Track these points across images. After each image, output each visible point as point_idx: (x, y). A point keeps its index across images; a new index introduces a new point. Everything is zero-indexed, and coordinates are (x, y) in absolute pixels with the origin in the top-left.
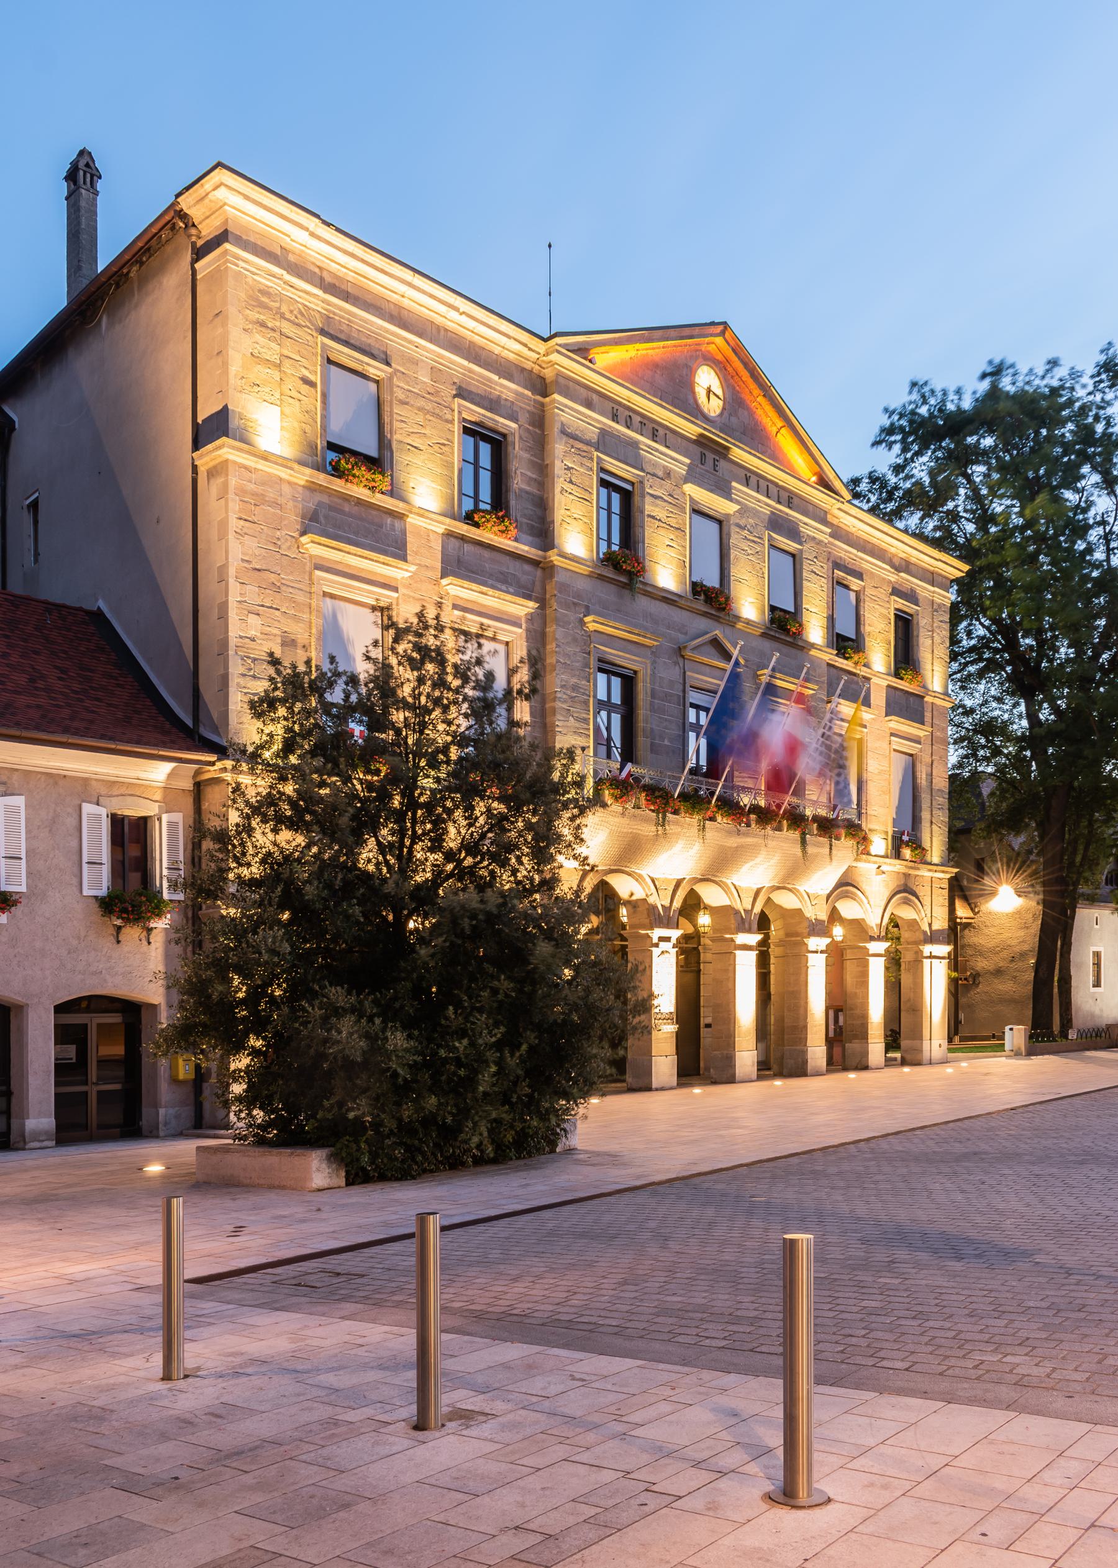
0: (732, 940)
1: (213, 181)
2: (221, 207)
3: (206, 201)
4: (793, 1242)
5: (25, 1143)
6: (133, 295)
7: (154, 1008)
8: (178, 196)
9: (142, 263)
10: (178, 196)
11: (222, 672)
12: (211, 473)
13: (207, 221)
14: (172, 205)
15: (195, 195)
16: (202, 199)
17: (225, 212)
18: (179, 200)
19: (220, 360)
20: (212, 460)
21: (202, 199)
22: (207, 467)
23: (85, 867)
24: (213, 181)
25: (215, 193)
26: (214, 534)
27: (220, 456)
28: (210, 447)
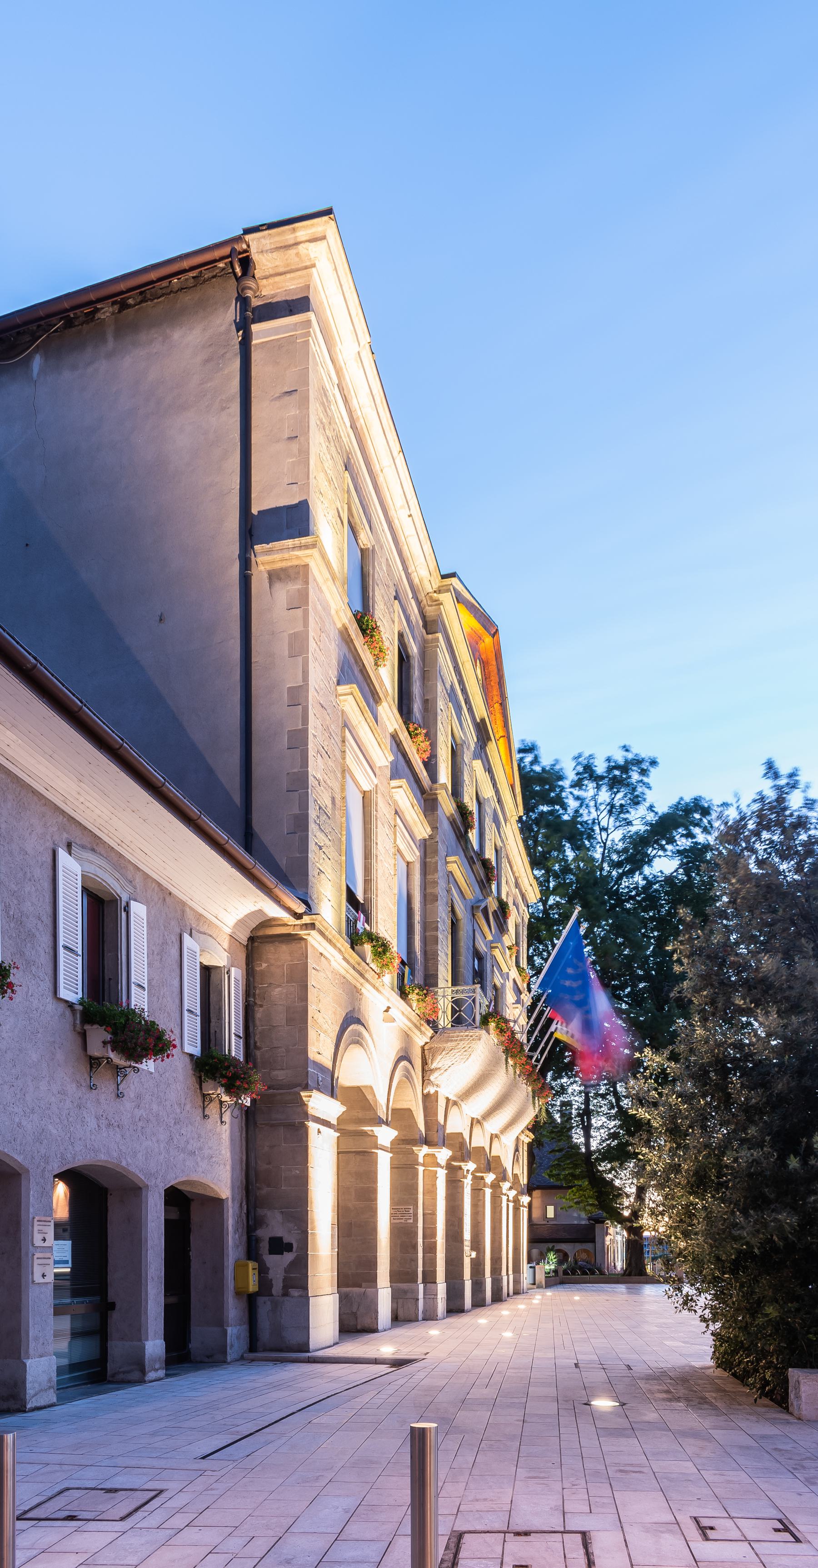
0: (460, 1168)
1: (313, 230)
2: (306, 268)
3: (292, 252)
4: (423, 1430)
5: (143, 1372)
6: (104, 340)
7: (218, 1202)
8: (247, 231)
9: (124, 306)
10: (247, 231)
11: (296, 811)
12: (275, 576)
13: (277, 279)
14: (238, 239)
15: (277, 239)
16: (287, 247)
17: (310, 276)
18: (248, 237)
19: (294, 446)
20: (282, 560)
21: (287, 247)
22: (268, 567)
23: (186, 1013)
24: (313, 230)
25: (311, 245)
26: (282, 648)
27: (298, 557)
28: (289, 542)
